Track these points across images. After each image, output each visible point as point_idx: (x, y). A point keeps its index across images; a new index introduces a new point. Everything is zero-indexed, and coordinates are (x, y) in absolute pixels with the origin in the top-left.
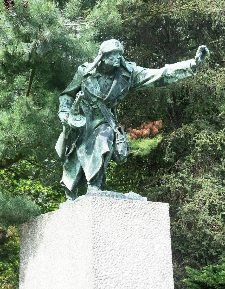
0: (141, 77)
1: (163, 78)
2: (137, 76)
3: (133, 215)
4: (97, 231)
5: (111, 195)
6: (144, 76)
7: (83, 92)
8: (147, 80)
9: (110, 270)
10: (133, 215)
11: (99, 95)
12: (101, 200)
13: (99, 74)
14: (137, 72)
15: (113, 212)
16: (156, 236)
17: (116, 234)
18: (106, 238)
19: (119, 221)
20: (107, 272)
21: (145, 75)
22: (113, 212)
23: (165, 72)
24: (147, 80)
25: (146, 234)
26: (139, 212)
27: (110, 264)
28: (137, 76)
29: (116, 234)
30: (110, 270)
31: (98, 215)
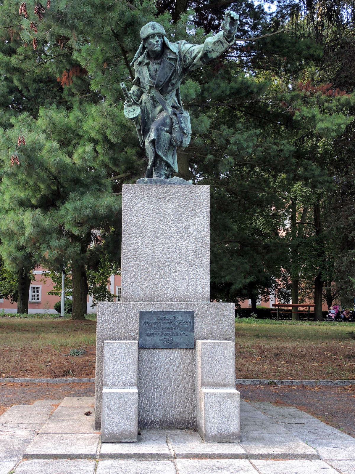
0: (188, 56)
1: (206, 53)
2: (185, 56)
3: (167, 199)
4: (128, 216)
5: (149, 182)
6: (192, 54)
7: (124, 84)
8: (195, 57)
9: (139, 250)
10: (167, 199)
11: (149, 82)
12: (132, 187)
13: (148, 61)
14: (184, 51)
15: (145, 198)
16: (192, 218)
17: (148, 218)
18: (137, 222)
19: (151, 206)
20: (137, 251)
21: (191, 53)
22: (145, 198)
23: (206, 47)
24: (195, 57)
25: (180, 216)
26: (174, 196)
27: (139, 245)
28: (185, 56)
29: (148, 218)
30: (139, 250)
31: (129, 202)
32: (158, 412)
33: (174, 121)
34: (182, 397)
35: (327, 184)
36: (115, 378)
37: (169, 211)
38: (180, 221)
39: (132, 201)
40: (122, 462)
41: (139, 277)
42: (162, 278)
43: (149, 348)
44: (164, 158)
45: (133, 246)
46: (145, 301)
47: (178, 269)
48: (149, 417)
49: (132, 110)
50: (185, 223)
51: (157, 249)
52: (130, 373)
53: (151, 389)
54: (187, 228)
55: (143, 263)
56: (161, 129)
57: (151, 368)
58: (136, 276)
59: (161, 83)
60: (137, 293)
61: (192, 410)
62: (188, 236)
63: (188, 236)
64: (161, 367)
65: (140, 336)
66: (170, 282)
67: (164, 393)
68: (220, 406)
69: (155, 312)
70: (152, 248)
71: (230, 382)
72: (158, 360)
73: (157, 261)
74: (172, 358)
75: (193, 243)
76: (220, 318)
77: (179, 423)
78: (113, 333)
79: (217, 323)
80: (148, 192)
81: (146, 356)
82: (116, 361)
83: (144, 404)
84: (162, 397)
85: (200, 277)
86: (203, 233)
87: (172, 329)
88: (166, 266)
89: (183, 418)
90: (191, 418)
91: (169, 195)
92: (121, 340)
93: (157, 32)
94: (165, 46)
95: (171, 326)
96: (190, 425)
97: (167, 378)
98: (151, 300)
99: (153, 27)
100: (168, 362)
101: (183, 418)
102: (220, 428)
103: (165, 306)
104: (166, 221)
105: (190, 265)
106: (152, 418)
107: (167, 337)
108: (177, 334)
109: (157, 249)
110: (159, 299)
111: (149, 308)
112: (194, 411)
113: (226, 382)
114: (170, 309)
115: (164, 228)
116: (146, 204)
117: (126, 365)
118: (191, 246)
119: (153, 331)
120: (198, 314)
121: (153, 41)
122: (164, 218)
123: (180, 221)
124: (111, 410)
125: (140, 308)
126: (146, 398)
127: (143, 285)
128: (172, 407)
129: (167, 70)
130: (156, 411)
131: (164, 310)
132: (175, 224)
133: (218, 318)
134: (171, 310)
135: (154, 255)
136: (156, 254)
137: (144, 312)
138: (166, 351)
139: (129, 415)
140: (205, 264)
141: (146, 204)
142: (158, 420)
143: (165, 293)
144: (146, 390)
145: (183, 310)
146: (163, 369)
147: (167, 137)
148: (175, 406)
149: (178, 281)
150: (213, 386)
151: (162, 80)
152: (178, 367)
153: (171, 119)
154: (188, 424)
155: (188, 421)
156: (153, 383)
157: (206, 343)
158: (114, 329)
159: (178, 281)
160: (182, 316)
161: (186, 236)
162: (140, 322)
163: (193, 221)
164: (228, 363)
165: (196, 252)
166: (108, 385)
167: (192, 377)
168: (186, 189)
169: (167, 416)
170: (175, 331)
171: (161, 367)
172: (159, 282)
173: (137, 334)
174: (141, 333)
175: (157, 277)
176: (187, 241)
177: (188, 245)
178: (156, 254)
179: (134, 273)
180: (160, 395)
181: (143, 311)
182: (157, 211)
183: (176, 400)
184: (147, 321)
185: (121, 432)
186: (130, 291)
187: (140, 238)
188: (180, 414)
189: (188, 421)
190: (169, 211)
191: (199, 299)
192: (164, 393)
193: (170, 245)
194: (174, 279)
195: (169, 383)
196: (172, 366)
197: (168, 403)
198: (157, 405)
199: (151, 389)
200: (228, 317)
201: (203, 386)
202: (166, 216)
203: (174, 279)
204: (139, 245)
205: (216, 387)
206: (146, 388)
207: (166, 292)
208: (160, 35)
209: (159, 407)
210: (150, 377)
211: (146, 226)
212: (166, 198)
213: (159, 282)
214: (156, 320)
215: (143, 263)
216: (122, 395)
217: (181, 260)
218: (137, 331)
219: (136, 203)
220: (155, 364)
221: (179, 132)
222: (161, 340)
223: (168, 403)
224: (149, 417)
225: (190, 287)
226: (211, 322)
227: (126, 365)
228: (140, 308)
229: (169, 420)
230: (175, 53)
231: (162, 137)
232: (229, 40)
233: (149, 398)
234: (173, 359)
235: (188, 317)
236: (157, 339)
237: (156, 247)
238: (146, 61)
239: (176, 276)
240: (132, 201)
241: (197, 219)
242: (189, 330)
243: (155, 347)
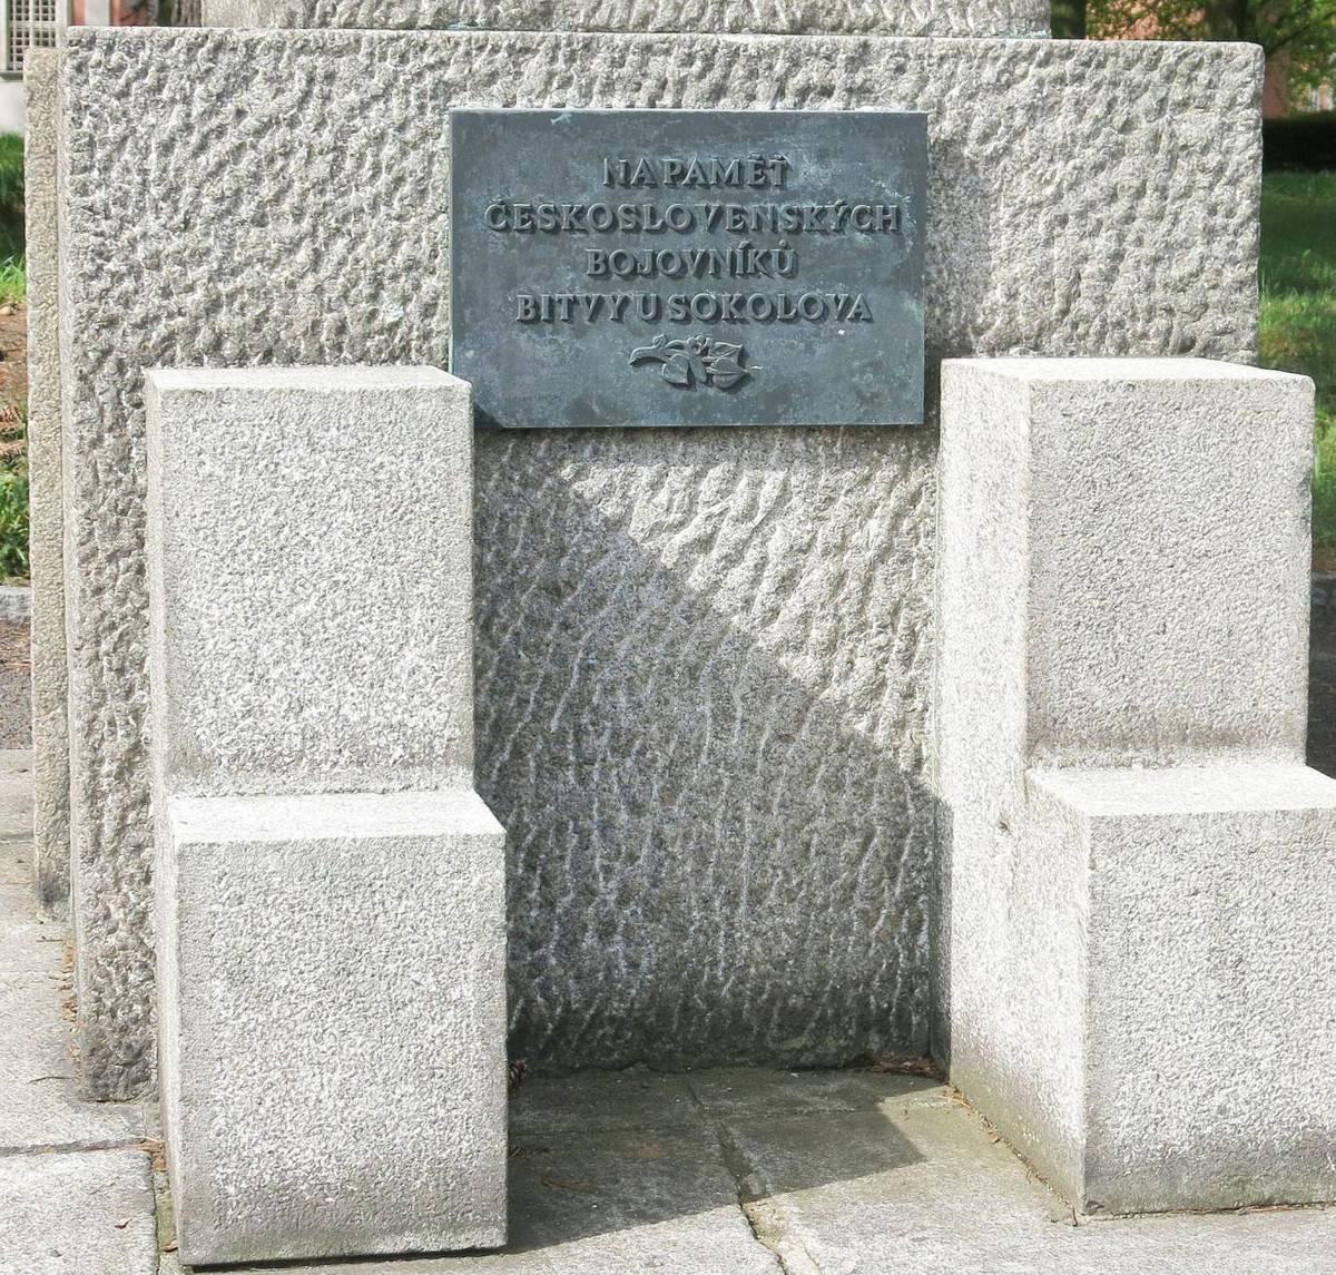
32: (617, 946)
34: (819, 823)
36: (275, 701)
40: (255, 1257)
46: (491, 25)
48: (544, 989)
52: (411, 656)
53: (560, 762)
61: (894, 920)
65: (460, 330)
67: (670, 793)
68: (1225, 916)
69: (585, 122)
71: (1264, 707)
77: (794, 1021)
78: (214, 306)
81: (515, 499)
82: (276, 559)
84: (647, 823)
89: (822, 982)
90: (888, 980)
92: (291, 359)
96: (884, 1031)
97: (693, 672)
101: (822, 982)
102: (1218, 1099)
103: (669, 67)
106: (565, 992)
108: (784, 314)
112: (915, 928)
113: (1234, 712)
117: (373, 587)
119: (571, 283)
124: (263, 998)
128: (732, 900)
130: (606, 932)
137: (490, 117)
139: (433, 1029)
142: (617, 1008)
145: (831, 106)
146: (657, 603)
148: (757, 896)
150: (1124, 741)
152: (786, 584)
154: (864, 1027)
155: (863, 1001)
157: (1077, 390)
160: (822, 156)
162: (459, 210)
164: (1255, 552)
166: (210, 762)
167: (907, 661)
169: (696, 975)
170: (772, 287)
173: (428, 310)
174: (463, 299)
180: (636, 808)
181: (477, 105)
183: (764, 845)
184: (522, 196)
185: (365, 1179)
188: (799, 954)
189: (863, 1001)
192: (670, 793)
195: (706, 708)
197: (698, 873)
198: (608, 889)
199: (560, 762)
201: (1042, 749)
205: (1147, 754)
206: (517, 753)
209: (622, 901)
210: (546, 666)
214: (599, 185)
216: (358, 859)
218: (436, 283)
220: (592, 559)
223: (698, 873)
224: (544, 989)
227: (373, 587)
229: (712, 1002)
233: (542, 834)
234: (748, 515)
235: (877, 165)
242: (884, 275)
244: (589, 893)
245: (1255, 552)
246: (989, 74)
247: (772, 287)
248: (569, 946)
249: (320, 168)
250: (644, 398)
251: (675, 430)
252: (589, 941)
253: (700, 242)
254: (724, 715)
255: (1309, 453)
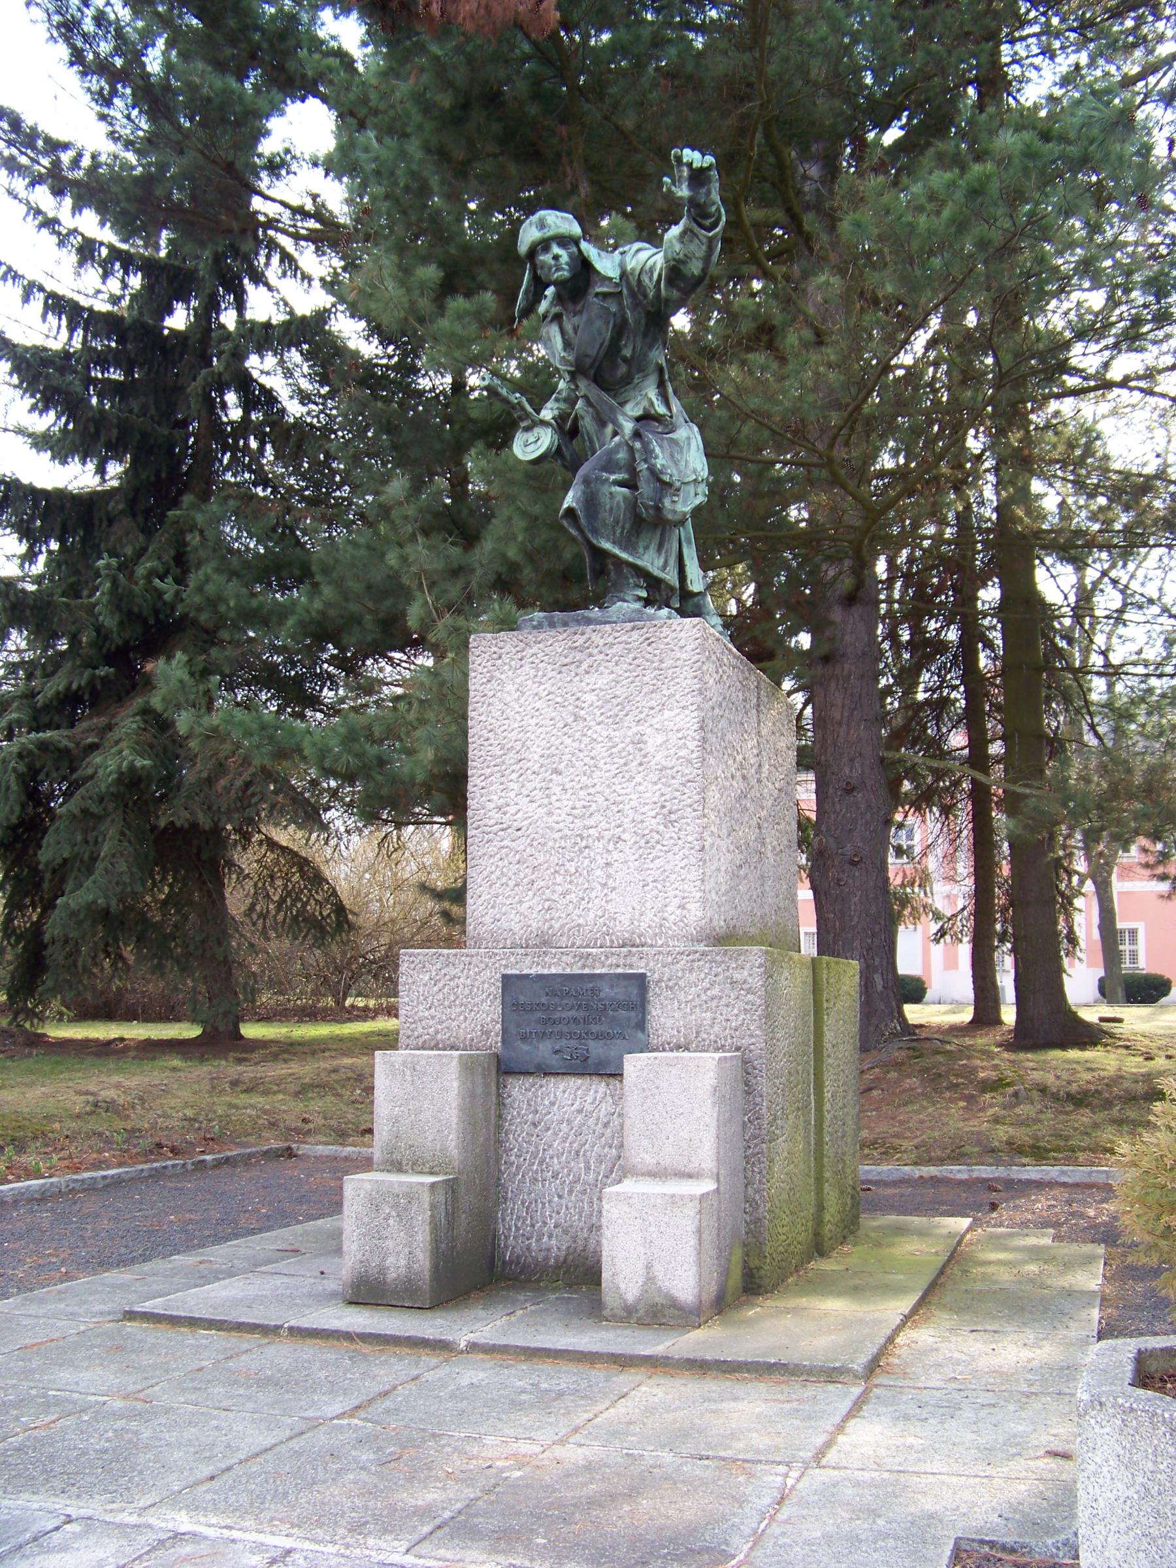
0: (645, 279)
10: (585, 666)
14: (633, 270)
15: (527, 668)
17: (533, 722)
22: (527, 668)
26: (602, 656)
28: (639, 281)
29: (533, 722)
30: (512, 809)
32: (553, 1242)
33: (637, 456)
35: (1106, 579)
37: (589, 698)
38: (616, 722)
39: (492, 677)
41: (512, 883)
42: (571, 882)
43: (531, 1074)
44: (624, 555)
45: (495, 798)
47: (616, 855)
49: (532, 439)
50: (634, 730)
51: (558, 804)
54: (639, 742)
55: (520, 845)
56: (598, 479)
57: (535, 1125)
58: (504, 880)
59: (588, 361)
60: (505, 925)
62: (641, 764)
63: (641, 764)
64: (561, 1122)
66: (593, 894)
67: (571, 1192)
70: (546, 801)
72: (553, 1104)
73: (557, 835)
74: (589, 1099)
75: (655, 783)
76: (722, 991)
78: (437, 1032)
79: (714, 1003)
80: (535, 650)
83: (518, 1218)
84: (564, 1202)
85: (673, 876)
86: (683, 753)
87: (586, 1021)
88: (581, 851)
91: (591, 655)
93: (551, 233)
94: (584, 266)
95: (581, 1014)
97: (577, 1153)
98: (545, 943)
99: (542, 225)
100: (580, 1111)
103: (569, 959)
104: (581, 724)
105: (648, 844)
107: (573, 1043)
108: (598, 1037)
109: (558, 804)
110: (564, 941)
111: (529, 967)
114: (584, 966)
115: (576, 745)
116: (529, 682)
118: (651, 793)
120: (660, 981)
121: (546, 258)
122: (577, 718)
123: (616, 722)
125: (506, 966)
126: (523, 1203)
127: (521, 902)
129: (599, 323)
130: (550, 1237)
131: (568, 971)
132: (605, 734)
133: (715, 991)
134: (587, 971)
135: (550, 820)
136: (555, 818)
138: (574, 1082)
140: (690, 839)
141: (529, 682)
143: (579, 925)
144: (522, 1181)
145: (620, 971)
147: (619, 498)
149: (614, 889)
151: (589, 352)
152: (606, 1125)
153: (631, 450)
156: (541, 1163)
158: (441, 1022)
159: (614, 889)
161: (635, 763)
163: (655, 720)
165: (663, 807)
168: (635, 635)
170: (595, 1028)
171: (561, 1122)
172: (564, 894)
175: (559, 879)
176: (639, 779)
177: (641, 788)
178: (555, 818)
179: (498, 873)
180: (560, 1197)
181: (509, 972)
182: (559, 699)
186: (487, 919)
187: (514, 776)
190: (589, 698)
191: (673, 937)
192: (571, 1192)
193: (592, 790)
194: (604, 885)
196: (591, 1122)
200: (745, 986)
202: (582, 713)
203: (604, 885)
204: (512, 794)
207: (581, 921)
208: (564, 240)
210: (532, 1149)
211: (529, 743)
212: (581, 662)
213: (564, 894)
215: (520, 845)
217: (624, 831)
219: (502, 683)
221: (648, 482)
222: (556, 1052)
225: (648, 905)
226: (697, 1002)
228: (506, 966)
230: (610, 279)
231: (605, 500)
232: (707, 223)
236: (544, 1050)
237: (554, 798)
238: (557, 309)
239: (609, 876)
240: (492, 677)
241: (667, 714)
243: (547, 1072)
244: (545, 1223)
245: (698, 1113)
246: (670, 959)
247: (595, 1028)
248: (539, 1240)
249: (467, 991)
250: (554, 1061)
251: (820, 1143)
252: (545, 1239)
253: (573, 1013)
254: (588, 1168)
255: (402, 1271)
